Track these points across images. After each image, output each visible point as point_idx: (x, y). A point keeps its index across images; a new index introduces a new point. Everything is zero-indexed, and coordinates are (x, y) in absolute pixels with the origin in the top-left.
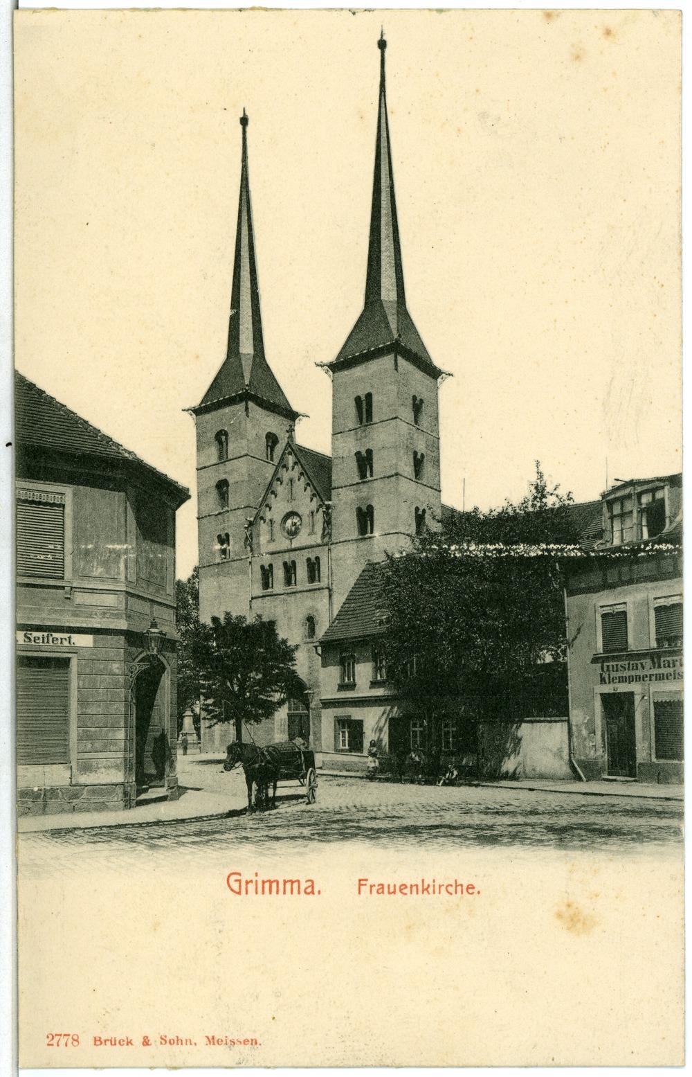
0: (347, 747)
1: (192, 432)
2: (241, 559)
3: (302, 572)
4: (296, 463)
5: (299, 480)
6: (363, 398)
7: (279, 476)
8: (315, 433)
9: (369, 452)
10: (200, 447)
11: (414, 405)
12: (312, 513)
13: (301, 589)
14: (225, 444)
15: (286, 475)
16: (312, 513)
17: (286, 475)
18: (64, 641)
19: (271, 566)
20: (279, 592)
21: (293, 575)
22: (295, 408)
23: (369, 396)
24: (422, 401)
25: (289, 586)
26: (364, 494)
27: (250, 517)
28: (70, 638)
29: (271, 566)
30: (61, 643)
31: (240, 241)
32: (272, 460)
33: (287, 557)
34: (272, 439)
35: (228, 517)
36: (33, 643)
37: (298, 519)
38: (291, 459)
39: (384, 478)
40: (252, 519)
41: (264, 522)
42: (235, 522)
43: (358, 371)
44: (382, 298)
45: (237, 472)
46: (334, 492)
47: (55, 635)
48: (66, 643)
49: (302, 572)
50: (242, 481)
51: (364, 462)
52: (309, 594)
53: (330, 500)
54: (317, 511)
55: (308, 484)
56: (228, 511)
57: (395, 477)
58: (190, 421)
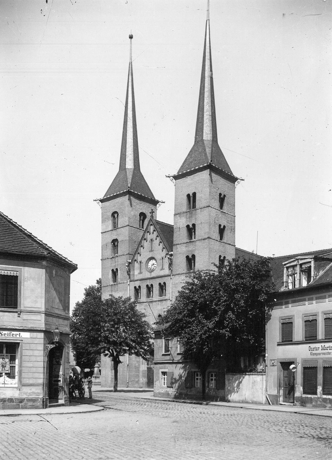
0: (166, 386)
1: (100, 211)
2: (124, 283)
3: (156, 290)
4: (154, 231)
5: (156, 239)
6: (191, 195)
7: (145, 237)
8: (165, 214)
9: (194, 225)
10: (103, 221)
11: (220, 198)
12: (163, 258)
13: (156, 300)
14: (117, 219)
15: (149, 237)
16: (163, 258)
17: (149, 237)
18: (17, 335)
19: (140, 287)
20: (144, 301)
21: (151, 292)
22: (157, 198)
23: (194, 194)
24: (225, 196)
25: (149, 298)
26: (190, 249)
27: (129, 260)
28: (20, 334)
29: (140, 287)
30: (16, 336)
31: (128, 99)
32: (143, 227)
33: (149, 283)
34: (143, 216)
35: (118, 260)
36: (3, 336)
37: (155, 261)
38: (152, 228)
39: (201, 240)
40: (130, 261)
41: (137, 263)
42: (121, 262)
43: (189, 180)
44: (204, 139)
45: (123, 235)
46: (174, 248)
47: (13, 333)
48: (18, 336)
49: (156, 290)
50: (126, 240)
51: (191, 230)
52: (159, 303)
53: (172, 251)
54: (165, 257)
55: (161, 242)
56: (117, 256)
57: (207, 239)
58: (98, 208)
